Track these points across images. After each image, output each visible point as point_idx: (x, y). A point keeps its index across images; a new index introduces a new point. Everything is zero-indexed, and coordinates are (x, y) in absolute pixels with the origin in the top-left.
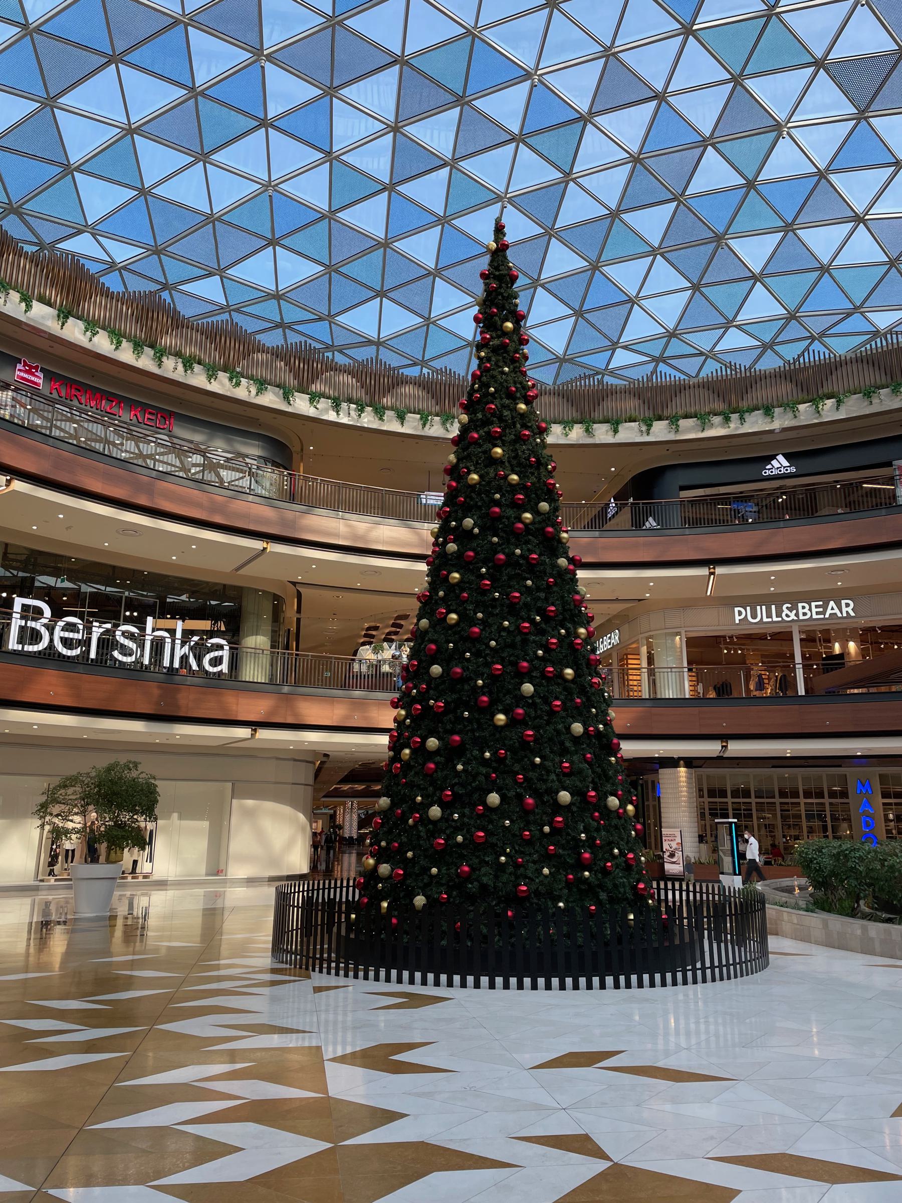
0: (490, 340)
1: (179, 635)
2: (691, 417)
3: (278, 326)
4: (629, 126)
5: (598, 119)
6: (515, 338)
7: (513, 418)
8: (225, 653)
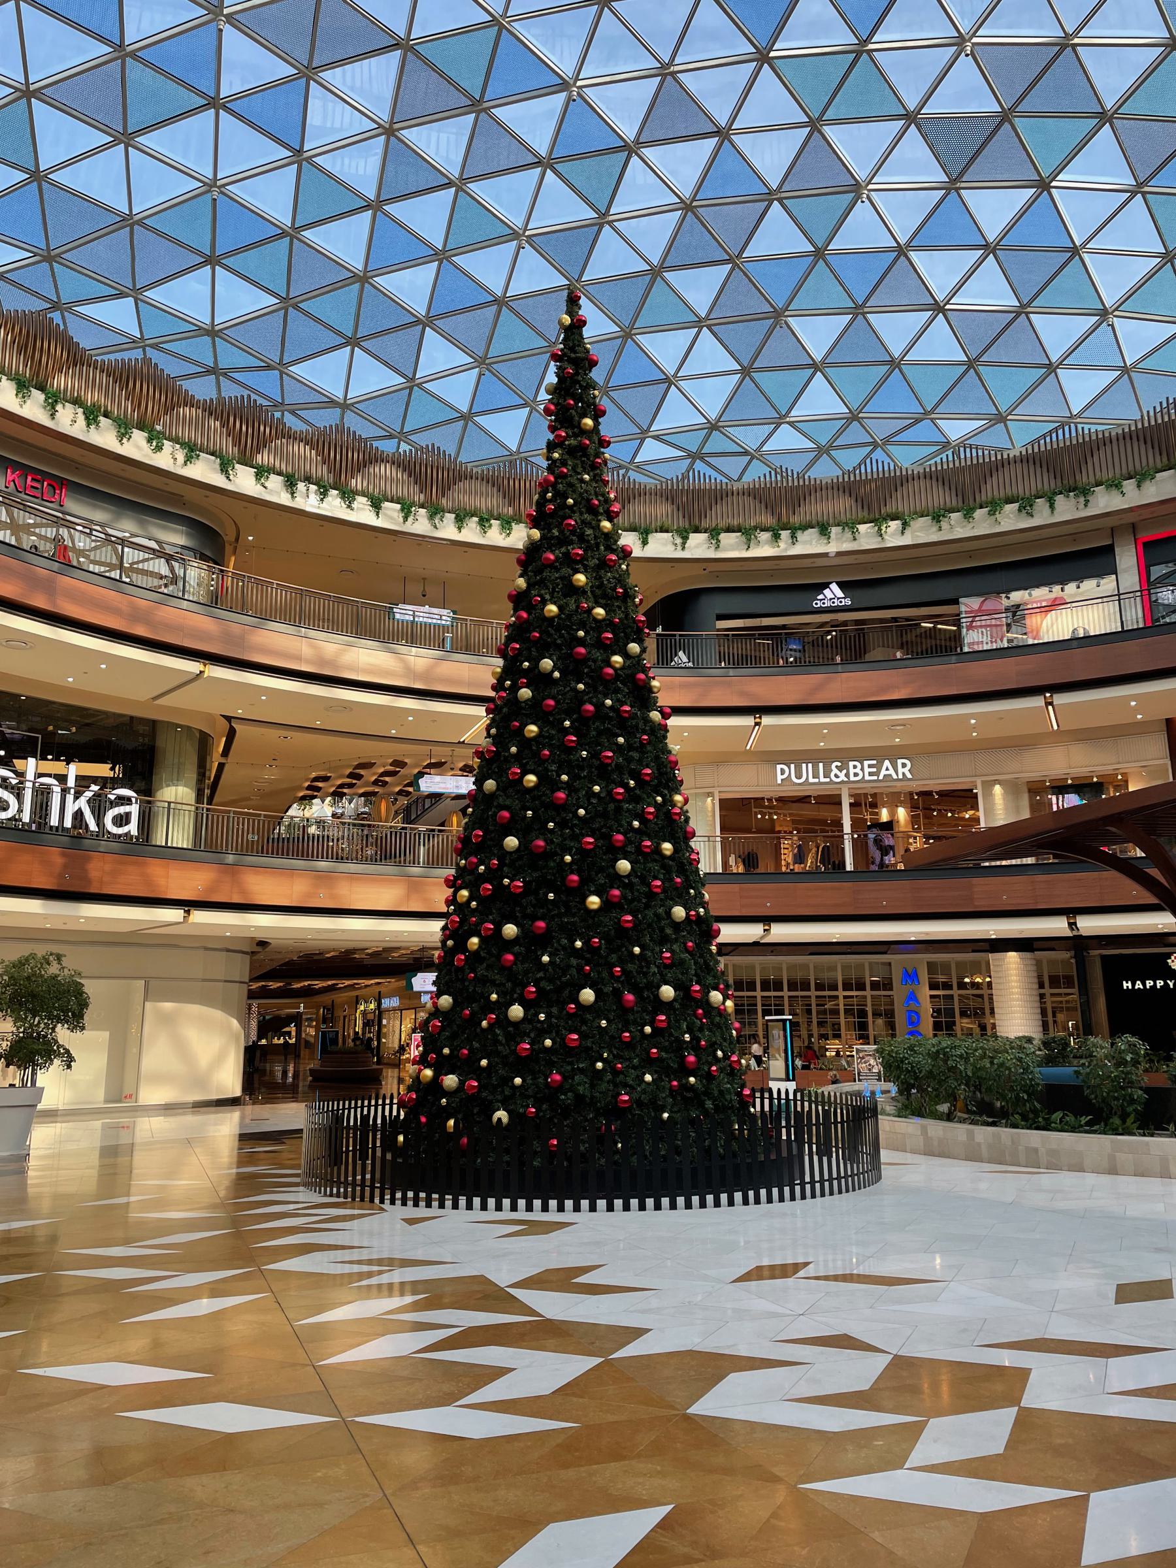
0: (565, 438)
1: (71, 782)
2: (734, 531)
3: (211, 371)
4: (683, 164)
5: (647, 152)
6: (596, 439)
7: (596, 537)
8: (134, 809)
